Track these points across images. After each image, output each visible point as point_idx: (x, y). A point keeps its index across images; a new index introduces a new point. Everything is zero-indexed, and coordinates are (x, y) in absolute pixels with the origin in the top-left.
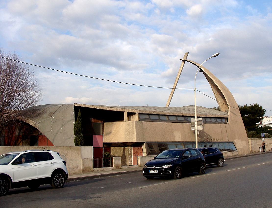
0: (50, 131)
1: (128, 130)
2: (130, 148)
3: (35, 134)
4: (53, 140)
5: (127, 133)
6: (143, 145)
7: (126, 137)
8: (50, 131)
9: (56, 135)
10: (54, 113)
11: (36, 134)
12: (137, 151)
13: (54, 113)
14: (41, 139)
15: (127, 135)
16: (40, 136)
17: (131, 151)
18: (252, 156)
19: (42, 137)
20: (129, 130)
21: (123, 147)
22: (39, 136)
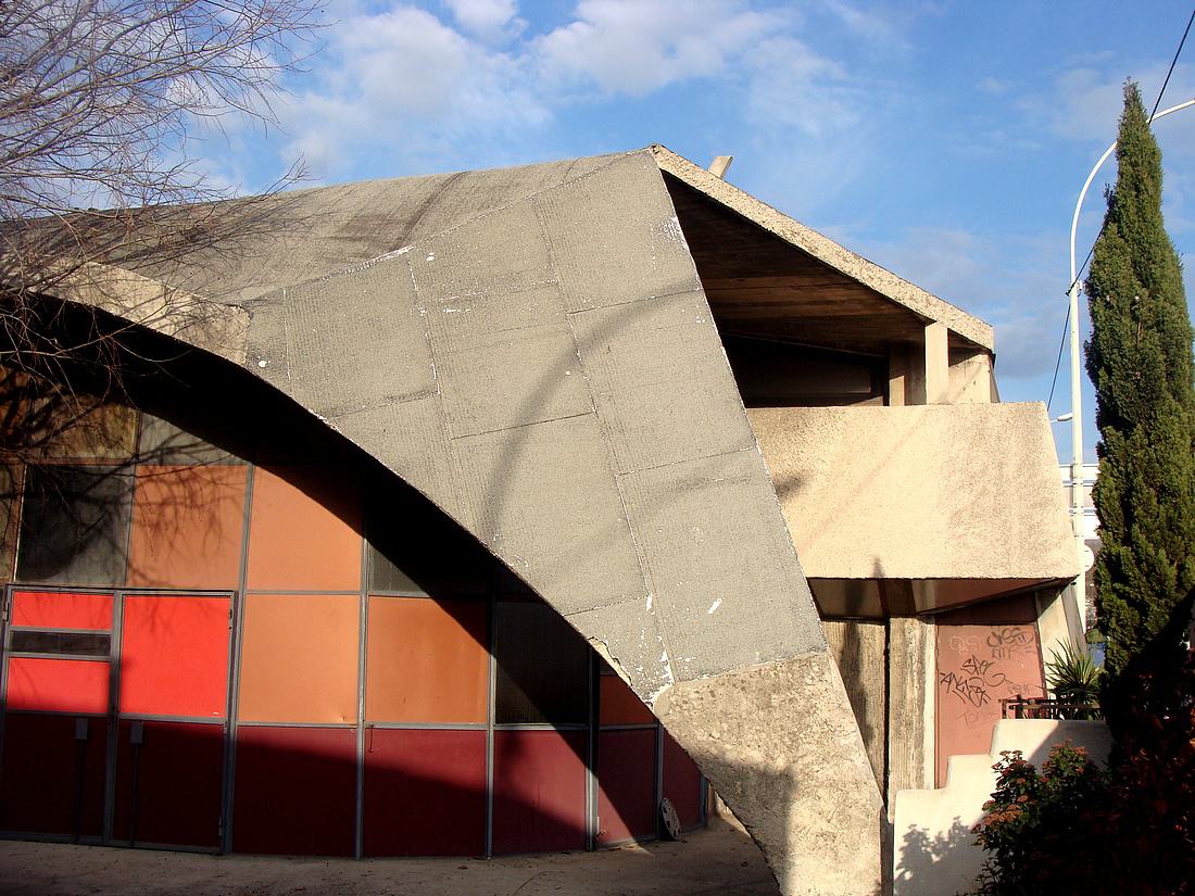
0: (423, 393)
1: (984, 472)
2: (917, 633)
3: (84, 454)
4: (493, 504)
5: (965, 498)
6: (1044, 607)
7: (960, 530)
8: (423, 393)
9: (511, 450)
10: (421, 212)
11: (101, 450)
12: (984, 654)
13: (407, 217)
14: (164, 504)
15: (974, 516)
16: (149, 477)
17: (921, 661)
18: (41, 636)
19: (182, 481)
20: (993, 473)
21: (841, 624)
22: (140, 470)
